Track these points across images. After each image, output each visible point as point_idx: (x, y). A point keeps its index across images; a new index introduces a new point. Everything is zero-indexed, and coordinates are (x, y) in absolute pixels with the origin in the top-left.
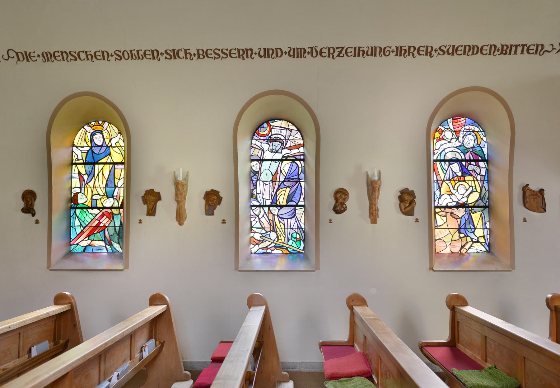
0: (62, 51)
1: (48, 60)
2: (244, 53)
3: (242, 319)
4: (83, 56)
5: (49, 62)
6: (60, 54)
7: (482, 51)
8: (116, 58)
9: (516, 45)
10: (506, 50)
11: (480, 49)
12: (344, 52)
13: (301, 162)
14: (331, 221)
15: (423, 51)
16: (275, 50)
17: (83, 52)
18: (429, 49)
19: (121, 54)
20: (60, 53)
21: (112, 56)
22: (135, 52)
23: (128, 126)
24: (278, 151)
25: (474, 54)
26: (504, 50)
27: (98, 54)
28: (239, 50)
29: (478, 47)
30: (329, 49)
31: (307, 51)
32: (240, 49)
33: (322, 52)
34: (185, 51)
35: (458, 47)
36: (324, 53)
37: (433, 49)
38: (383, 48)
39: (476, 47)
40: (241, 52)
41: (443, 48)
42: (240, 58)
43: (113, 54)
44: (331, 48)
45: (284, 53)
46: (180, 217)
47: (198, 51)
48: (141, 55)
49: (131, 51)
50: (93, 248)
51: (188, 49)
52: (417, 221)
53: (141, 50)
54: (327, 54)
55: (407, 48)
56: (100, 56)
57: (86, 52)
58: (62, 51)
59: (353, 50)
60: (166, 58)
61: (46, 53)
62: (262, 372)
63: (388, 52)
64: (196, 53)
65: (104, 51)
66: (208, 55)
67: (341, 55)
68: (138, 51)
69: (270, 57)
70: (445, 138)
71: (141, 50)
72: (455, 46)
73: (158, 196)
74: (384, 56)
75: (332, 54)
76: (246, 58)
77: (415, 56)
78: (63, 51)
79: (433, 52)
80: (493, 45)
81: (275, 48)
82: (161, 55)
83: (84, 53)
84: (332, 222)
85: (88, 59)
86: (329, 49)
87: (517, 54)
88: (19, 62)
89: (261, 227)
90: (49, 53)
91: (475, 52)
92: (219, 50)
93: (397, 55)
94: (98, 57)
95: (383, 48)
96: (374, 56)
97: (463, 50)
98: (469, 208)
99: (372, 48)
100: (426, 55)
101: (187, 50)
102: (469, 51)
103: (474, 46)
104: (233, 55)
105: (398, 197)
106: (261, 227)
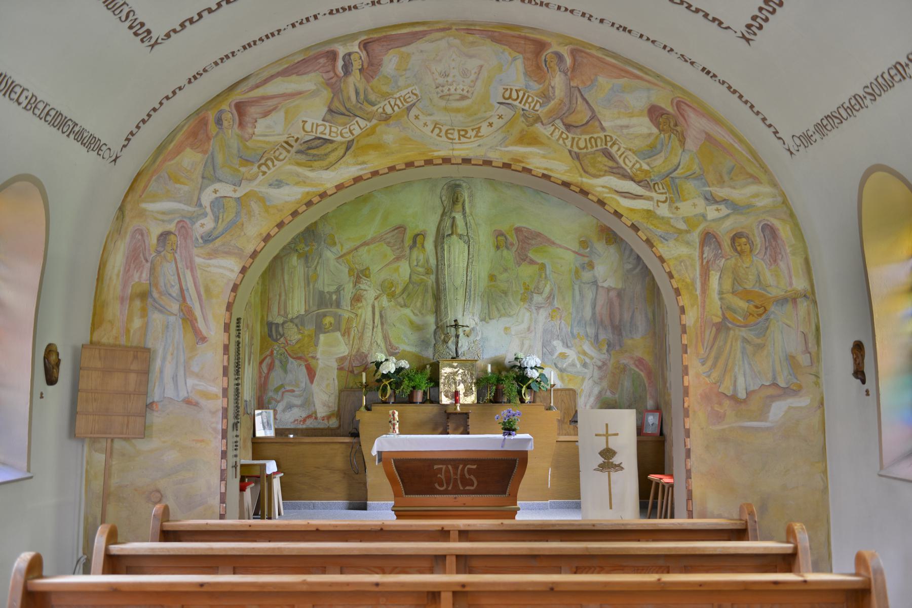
8: (871, 100)
19: (870, 91)
49: (876, 80)
68: (882, 76)
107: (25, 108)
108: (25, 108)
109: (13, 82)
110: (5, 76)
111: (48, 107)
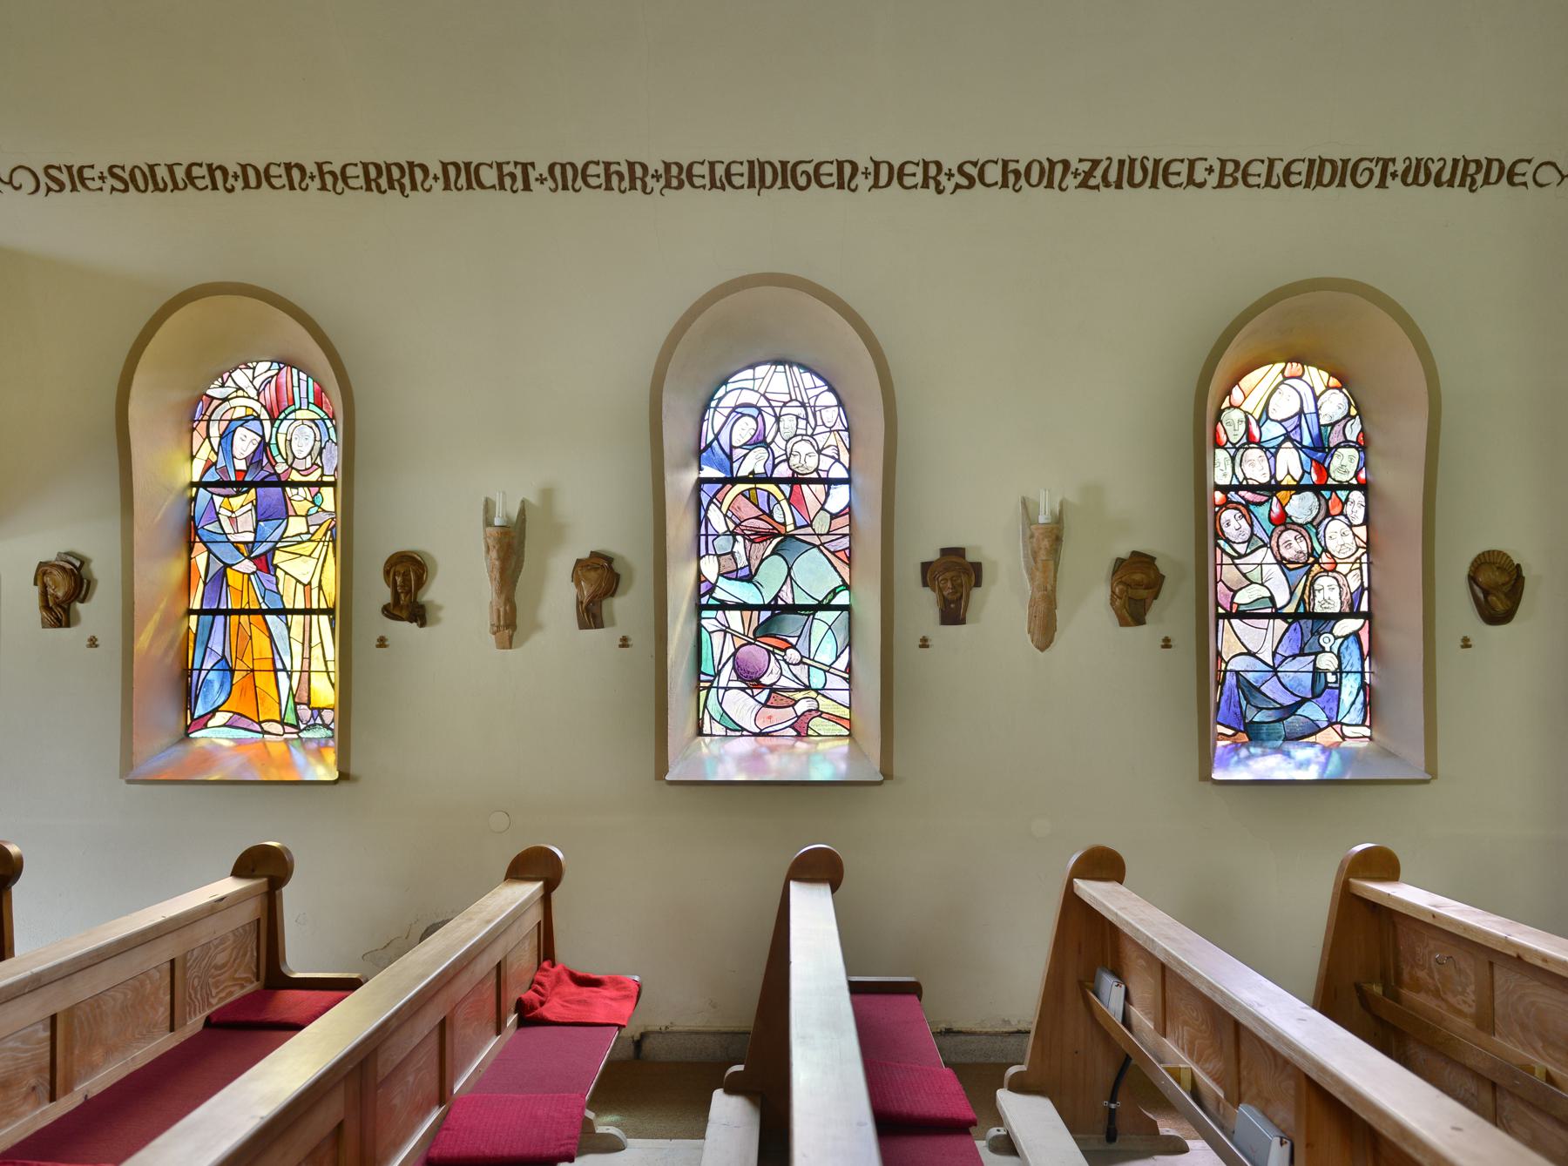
0: (413, 162)
1: (565, 188)
2: (403, 175)
3: (487, 888)
4: (993, 174)
5: (471, 191)
6: (282, 171)
7: (730, 178)
9: (608, 163)
10: (1343, 173)
11: (580, 171)
12: (1099, 172)
13: (780, 485)
14: (382, 642)
15: (831, 175)
16: (1046, 165)
17: (490, 166)
18: (933, 170)
20: (1187, 166)
21: (950, 175)
22: (162, 172)
23: (1201, 374)
24: (833, 457)
25: (1489, 184)
26: (931, 178)
27: (592, 170)
28: (365, 166)
29: (891, 167)
30: (926, 164)
31: (308, 174)
32: (369, 163)
33: (906, 172)
34: (1005, 163)
35: (1169, 164)
36: (354, 179)
37: (857, 170)
38: (580, 167)
39: (569, 168)
40: (373, 172)
41: (969, 169)
42: (395, 189)
43: (955, 171)
44: (846, 161)
45: (870, 174)
46: (1045, 630)
47: (667, 166)
48: (163, 178)
50: (848, 711)
51: (614, 163)
52: (93, 642)
53: (1282, 160)
54: (919, 179)
55: (624, 169)
56: (598, 176)
57: (500, 166)
58: (413, 162)
59: (745, 169)
60: (113, 189)
61: (563, 166)
62: (1375, 1034)
63: (1367, 174)
64: (661, 171)
65: (670, 163)
66: (86, 181)
67: (1092, 182)
68: (170, 168)
69: (419, 187)
70: (276, 425)
71: (1282, 160)
72: (1160, 160)
73: (975, 573)
74: (898, 186)
75: (934, 178)
76: (412, 189)
77: (648, 190)
78: (293, 164)
79: (650, 182)
80: (1473, 161)
81: (1486, 158)
82: (947, 177)
83: (494, 171)
84: (928, 647)
85: (502, 187)
86: (926, 164)
87: (531, 190)
88: (763, 191)
89: (1272, 665)
90: (573, 165)
91: (1326, 180)
92: (59, 169)
93: (447, 187)
94: (275, 182)
95: (580, 167)
96: (1304, 187)
97: (746, 175)
98: (227, 609)
99: (1456, 162)
100: (925, 185)
101: (1010, 163)
102: (574, 180)
103: (1490, 161)
104: (1251, 180)
105: (96, 581)
106: (1272, 665)
107: (1220, 185)
108: (1220, 185)
109: (1157, 162)
110: (1132, 161)
111: (1277, 163)
